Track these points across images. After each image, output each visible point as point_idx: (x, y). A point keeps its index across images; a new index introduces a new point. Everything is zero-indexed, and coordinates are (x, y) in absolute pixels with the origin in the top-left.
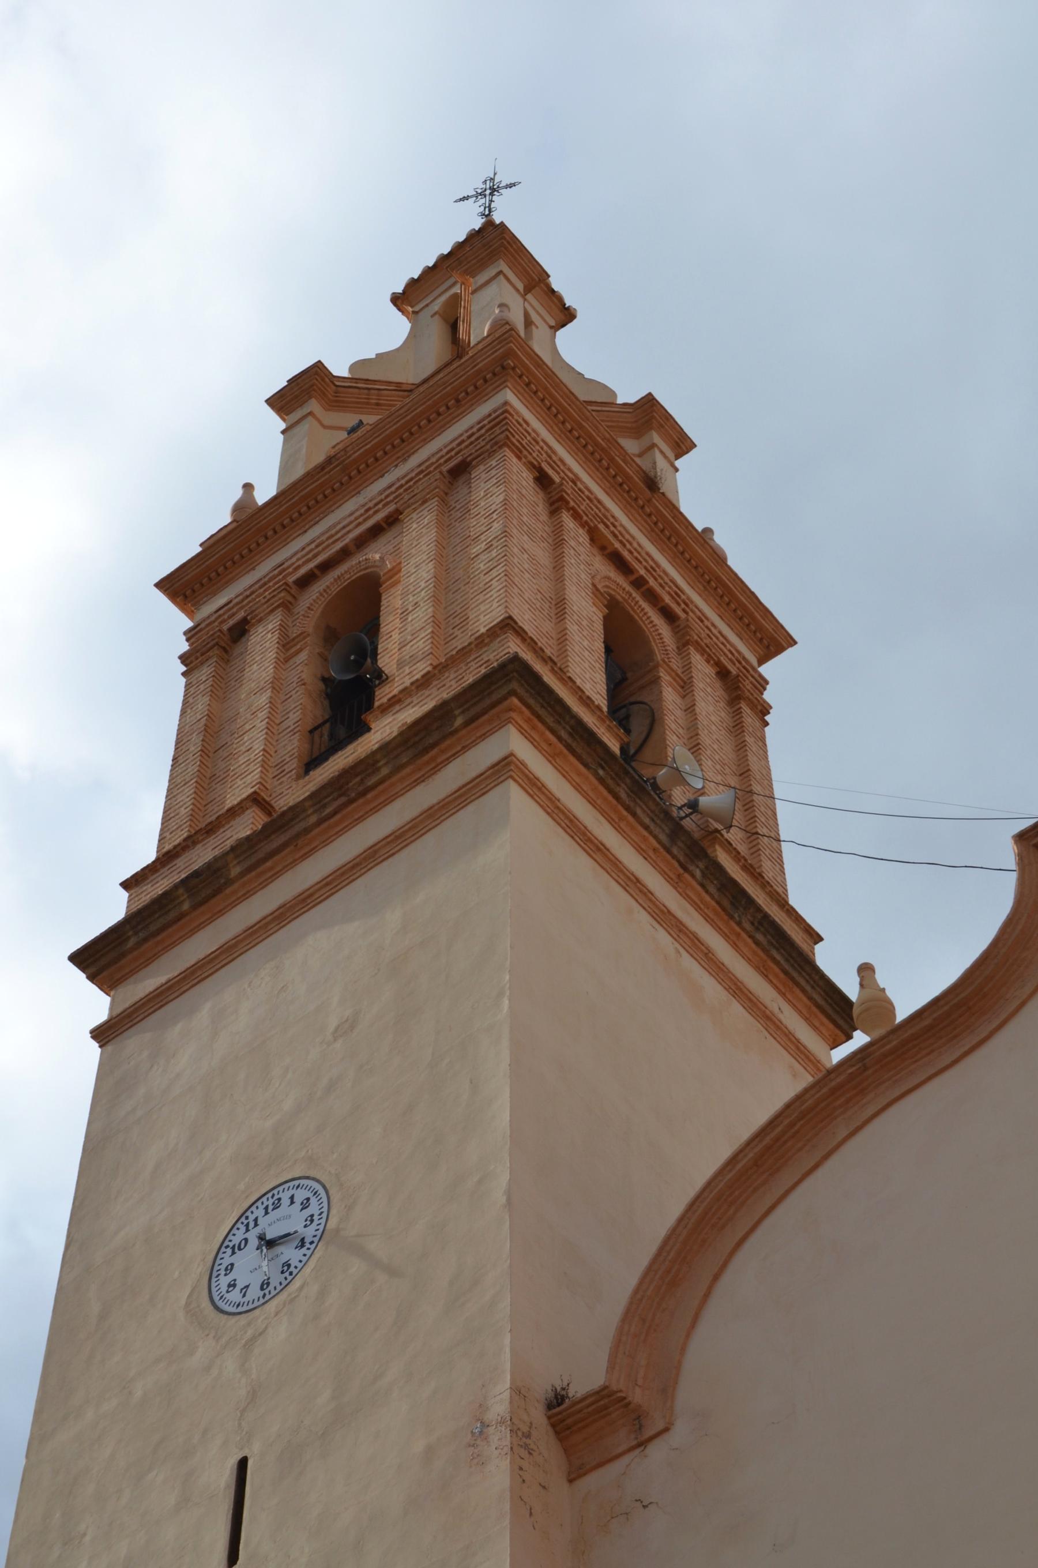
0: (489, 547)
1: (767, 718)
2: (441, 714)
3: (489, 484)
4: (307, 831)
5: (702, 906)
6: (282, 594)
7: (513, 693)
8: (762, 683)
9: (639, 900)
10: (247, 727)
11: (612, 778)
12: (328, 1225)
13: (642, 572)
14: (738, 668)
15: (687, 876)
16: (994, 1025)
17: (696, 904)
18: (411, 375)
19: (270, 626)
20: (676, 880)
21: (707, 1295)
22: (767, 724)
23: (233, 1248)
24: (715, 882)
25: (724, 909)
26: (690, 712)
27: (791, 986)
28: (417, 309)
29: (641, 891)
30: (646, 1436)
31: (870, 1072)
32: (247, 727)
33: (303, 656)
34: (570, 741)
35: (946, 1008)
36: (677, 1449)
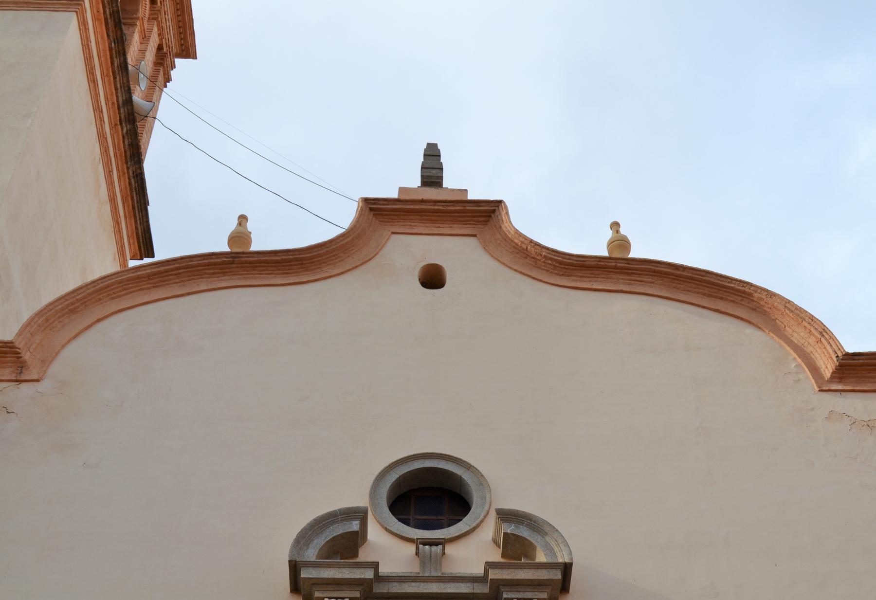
1: (167, 84)
5: (117, 148)
8: (173, 66)
9: (97, 122)
11: (116, 52)
14: (167, 50)
16: (311, 278)
17: (115, 145)
20: (113, 126)
22: (166, 86)
24: (130, 140)
25: (126, 156)
26: (142, 53)
27: (132, 216)
29: (100, 118)
30: (21, 379)
31: (234, 266)
34: (109, 17)
35: (291, 257)
36: (40, 393)
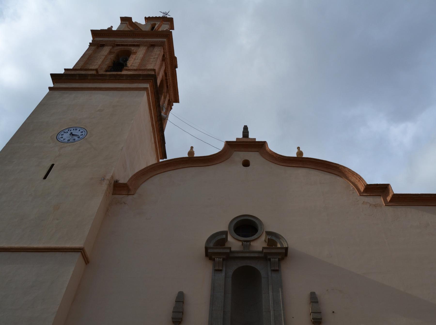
0: (154, 58)
2: (139, 75)
3: (158, 50)
4: (106, 79)
6: (113, 45)
7: (152, 79)
8: (173, 105)
10: (98, 59)
12: (85, 137)
13: (168, 78)
15: (157, 122)
18: (143, 29)
19: (109, 48)
21: (148, 179)
22: (171, 111)
23: (64, 132)
28: (148, 21)
32: (98, 59)
33: (113, 55)
